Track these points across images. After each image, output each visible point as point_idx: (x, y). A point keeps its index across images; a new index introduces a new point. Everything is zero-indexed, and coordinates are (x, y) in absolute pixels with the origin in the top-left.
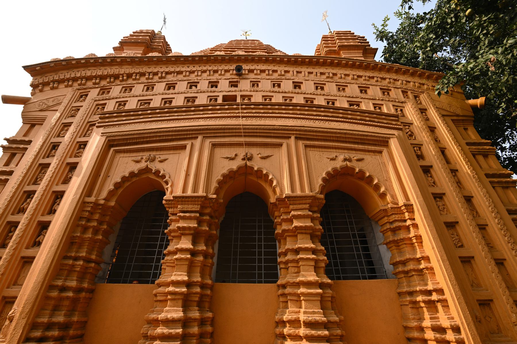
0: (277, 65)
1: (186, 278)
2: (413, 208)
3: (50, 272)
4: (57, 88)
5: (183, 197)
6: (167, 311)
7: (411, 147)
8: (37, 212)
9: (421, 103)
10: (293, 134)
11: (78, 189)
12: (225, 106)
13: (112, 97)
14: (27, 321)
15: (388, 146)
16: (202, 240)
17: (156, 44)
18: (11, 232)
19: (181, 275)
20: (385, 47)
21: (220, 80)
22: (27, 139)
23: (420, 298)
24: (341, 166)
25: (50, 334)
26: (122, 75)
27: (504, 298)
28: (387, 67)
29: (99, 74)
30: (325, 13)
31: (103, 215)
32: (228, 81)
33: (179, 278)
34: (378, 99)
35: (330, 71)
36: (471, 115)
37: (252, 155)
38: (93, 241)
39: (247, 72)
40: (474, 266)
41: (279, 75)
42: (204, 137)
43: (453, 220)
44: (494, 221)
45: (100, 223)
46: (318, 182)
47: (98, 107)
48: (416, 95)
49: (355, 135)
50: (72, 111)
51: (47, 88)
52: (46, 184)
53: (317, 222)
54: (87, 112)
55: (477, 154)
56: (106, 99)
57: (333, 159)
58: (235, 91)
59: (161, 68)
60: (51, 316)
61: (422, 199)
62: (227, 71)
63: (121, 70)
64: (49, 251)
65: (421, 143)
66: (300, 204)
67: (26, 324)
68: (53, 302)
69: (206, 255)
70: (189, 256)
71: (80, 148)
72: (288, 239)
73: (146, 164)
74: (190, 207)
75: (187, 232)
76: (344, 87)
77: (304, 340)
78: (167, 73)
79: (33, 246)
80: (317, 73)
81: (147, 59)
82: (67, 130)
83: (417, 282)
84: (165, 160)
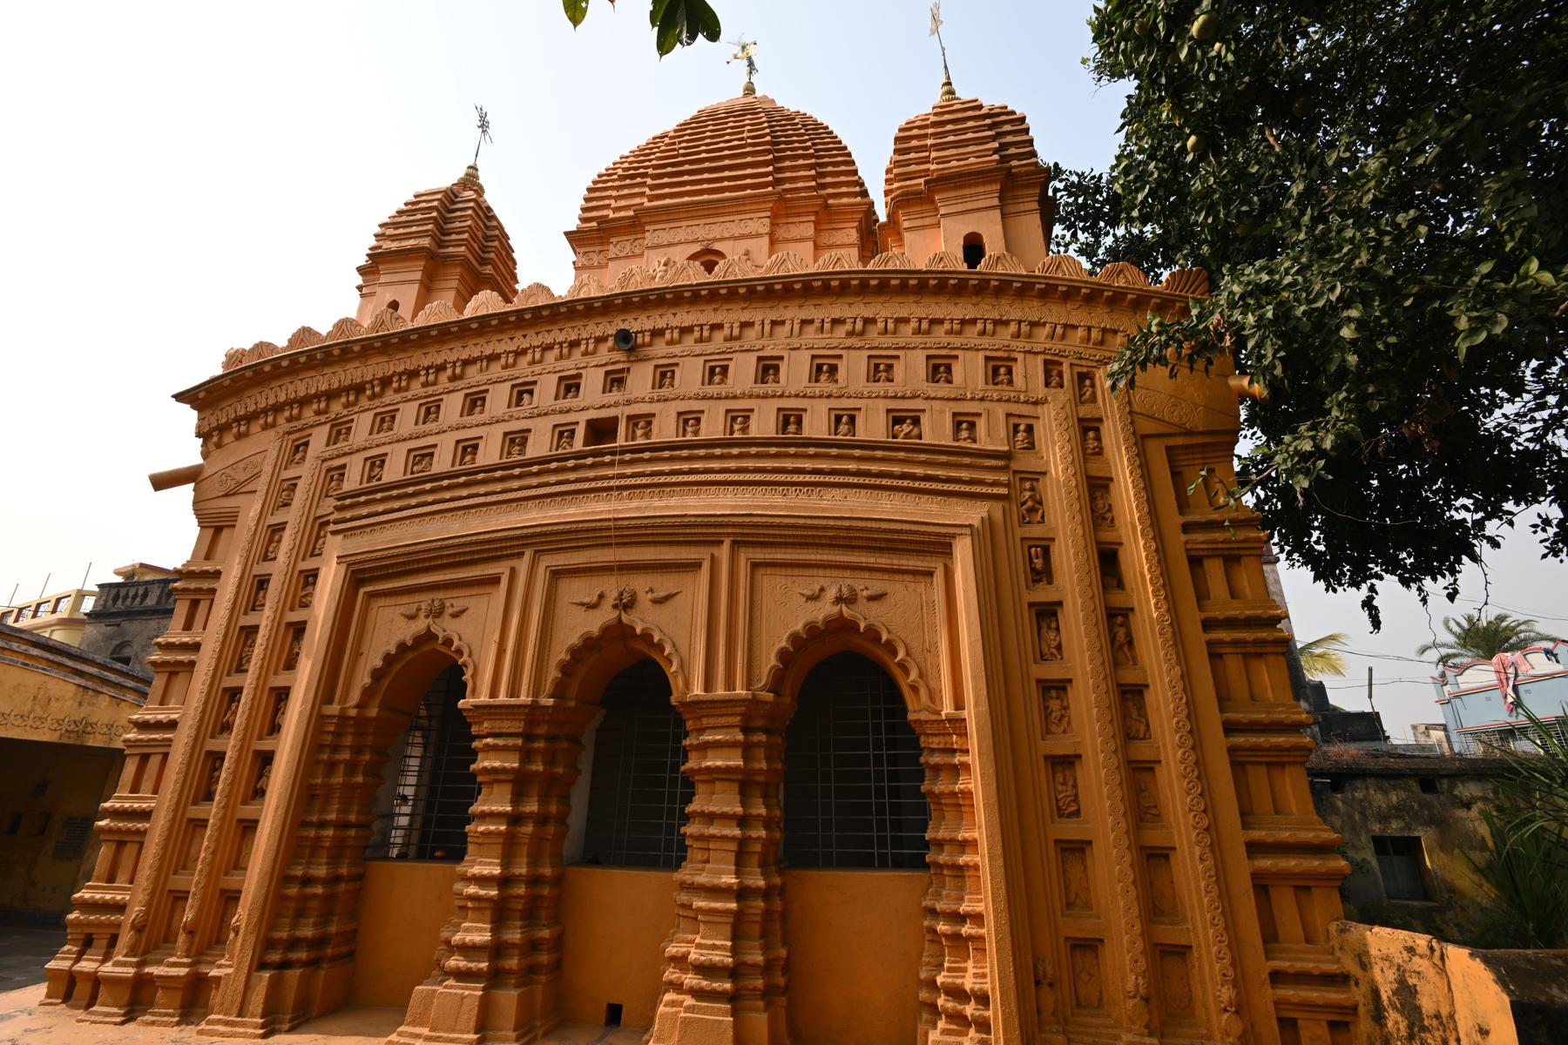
0: (725, 307)
1: (497, 871)
4: (246, 434)
5: (490, 707)
6: (467, 930)
10: (728, 534)
11: (307, 689)
12: (585, 457)
13: (355, 447)
14: (257, 938)
17: (454, 237)
18: (216, 770)
20: (1129, 97)
22: (209, 567)
24: (825, 618)
25: (295, 956)
26: (371, 382)
27: (1126, 938)
28: (1015, 285)
33: (486, 871)
34: (969, 396)
41: (725, 340)
43: (1070, 752)
44: (1175, 754)
46: (768, 661)
48: (1085, 370)
49: (870, 530)
51: (228, 438)
53: (760, 753)
54: (315, 477)
55: (1207, 557)
56: (345, 454)
57: (812, 598)
58: (616, 404)
59: (451, 349)
60: (294, 926)
62: (600, 340)
65: (1050, 536)
66: (722, 715)
68: (293, 905)
71: (306, 584)
73: (427, 621)
75: (502, 777)
78: (467, 363)
79: (253, 798)
82: (279, 541)
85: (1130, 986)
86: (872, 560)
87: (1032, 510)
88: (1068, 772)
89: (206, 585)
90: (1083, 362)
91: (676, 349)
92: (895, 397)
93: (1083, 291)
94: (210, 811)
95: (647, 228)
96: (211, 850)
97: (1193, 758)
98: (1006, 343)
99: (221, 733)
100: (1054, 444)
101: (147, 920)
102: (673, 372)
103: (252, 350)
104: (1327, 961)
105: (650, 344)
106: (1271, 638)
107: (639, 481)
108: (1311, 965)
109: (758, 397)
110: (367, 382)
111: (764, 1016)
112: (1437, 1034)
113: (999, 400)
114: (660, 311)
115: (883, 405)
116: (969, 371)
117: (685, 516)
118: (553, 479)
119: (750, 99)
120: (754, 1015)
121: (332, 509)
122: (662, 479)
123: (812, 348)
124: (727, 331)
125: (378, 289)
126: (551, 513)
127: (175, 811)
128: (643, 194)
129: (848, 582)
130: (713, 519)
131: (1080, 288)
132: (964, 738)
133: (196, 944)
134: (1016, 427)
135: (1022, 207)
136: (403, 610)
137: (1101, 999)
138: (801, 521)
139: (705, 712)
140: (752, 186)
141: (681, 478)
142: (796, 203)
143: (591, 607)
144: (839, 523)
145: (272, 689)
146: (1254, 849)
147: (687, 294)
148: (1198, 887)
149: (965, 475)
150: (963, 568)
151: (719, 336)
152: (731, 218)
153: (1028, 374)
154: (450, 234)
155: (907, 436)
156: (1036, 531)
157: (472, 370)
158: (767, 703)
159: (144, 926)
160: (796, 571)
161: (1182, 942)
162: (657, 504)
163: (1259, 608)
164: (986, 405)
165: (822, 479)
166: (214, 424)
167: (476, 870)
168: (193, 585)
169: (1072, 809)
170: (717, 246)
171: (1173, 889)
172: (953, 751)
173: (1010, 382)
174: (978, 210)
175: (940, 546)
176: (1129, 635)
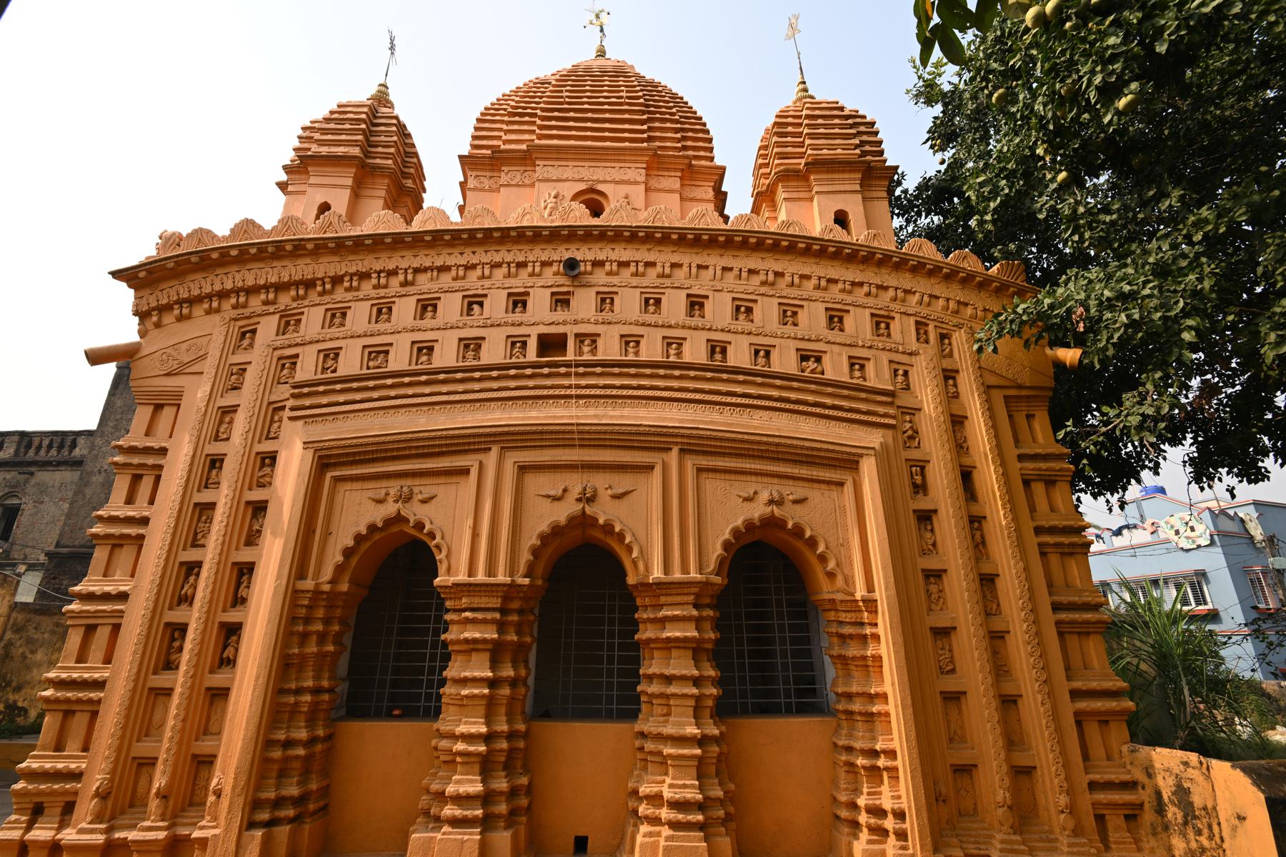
0: (657, 248)
1: (484, 729)
2: (876, 606)
3: (264, 721)
4: (189, 317)
6: (458, 782)
7: (904, 465)
8: (214, 606)
9: (951, 355)
10: (677, 443)
12: (541, 367)
13: (308, 339)
14: (245, 799)
15: (857, 469)
16: (507, 658)
17: (380, 149)
19: (475, 723)
20: (935, 118)
21: (530, 290)
23: (860, 761)
24: (760, 516)
26: (322, 279)
29: (273, 281)
30: (793, 21)
31: (330, 607)
32: (548, 292)
33: (473, 729)
34: (861, 344)
35: (769, 264)
36: (1048, 385)
37: (595, 491)
38: (322, 655)
39: (589, 268)
40: (964, 707)
41: (658, 276)
42: (502, 448)
43: (947, 624)
44: (1021, 627)
45: (327, 621)
46: (715, 551)
47: (284, 361)
48: (945, 331)
49: (795, 447)
50: (232, 374)
51: (168, 319)
52: (218, 551)
53: (707, 625)
54: (264, 380)
55: (1034, 480)
56: (297, 345)
57: (748, 500)
58: (564, 323)
59: (402, 257)
60: (278, 787)
61: (893, 592)
62: (545, 264)
63: (316, 266)
64: (255, 685)
66: (678, 594)
67: (244, 804)
68: (276, 766)
69: (513, 683)
70: (486, 691)
71: (263, 465)
72: (656, 653)
74: (483, 601)
75: (481, 646)
76: (795, 309)
77: (666, 827)
80: (741, 270)
81: (370, 242)
83: (860, 734)
84: (432, 498)
85: (1000, 798)
86: (796, 471)
87: (912, 438)
88: (944, 640)
89: (150, 461)
90: (944, 326)
91: (615, 280)
92: (802, 339)
93: (945, 270)
94: (175, 681)
95: (537, 163)
96: (181, 717)
97: (1034, 630)
98: (887, 304)
99: (179, 604)
100: (926, 387)
101: (111, 787)
102: (612, 299)
103: (190, 236)
104: (1122, 773)
105: (591, 273)
106: (1080, 542)
107: (593, 392)
108: (1114, 776)
109: (690, 328)
110: (318, 279)
111: (728, 840)
112: (1204, 820)
113: (883, 349)
114: (600, 245)
115: (794, 345)
116: (858, 323)
117: (640, 425)
118: (512, 384)
119: (601, 62)
120: (719, 839)
121: (287, 395)
122: (614, 392)
123: (732, 292)
124: (659, 269)
125: (309, 190)
126: (515, 415)
127: (136, 681)
128: (533, 132)
129: (777, 487)
130: (665, 430)
131: (943, 268)
132: (873, 615)
133: (170, 808)
134: (896, 371)
135: (875, 194)
136: (371, 494)
137: (975, 809)
138: (740, 436)
139: (664, 592)
140: (631, 140)
141: (630, 392)
142: (667, 160)
143: (557, 499)
144: (771, 440)
145: (234, 564)
146: (1076, 694)
147: (627, 234)
148: (1040, 724)
149: (863, 407)
150: (870, 481)
151: (652, 273)
152: (613, 165)
153: (902, 330)
154: (377, 146)
155: (813, 371)
156: (915, 454)
157: (422, 278)
158: (715, 585)
159: (109, 793)
160: (733, 477)
161: (1030, 764)
162: (612, 413)
163: (1072, 520)
164: (873, 352)
165: (751, 401)
166: (154, 304)
167: (462, 729)
168: (136, 460)
169: (949, 668)
170: (600, 187)
171: (1020, 725)
172: (862, 624)
173: (889, 335)
174: (845, 192)
175: (849, 462)
176: (982, 536)
